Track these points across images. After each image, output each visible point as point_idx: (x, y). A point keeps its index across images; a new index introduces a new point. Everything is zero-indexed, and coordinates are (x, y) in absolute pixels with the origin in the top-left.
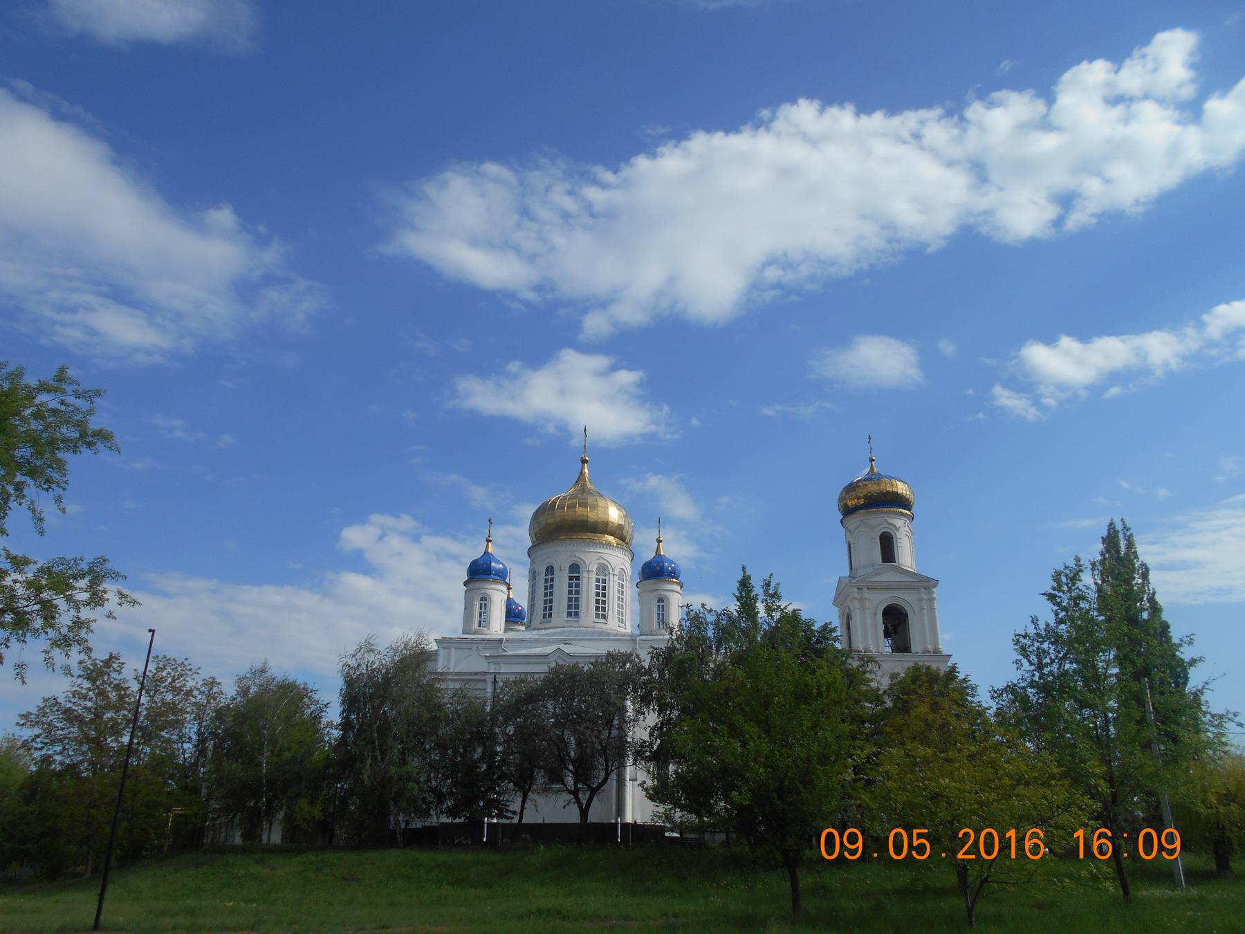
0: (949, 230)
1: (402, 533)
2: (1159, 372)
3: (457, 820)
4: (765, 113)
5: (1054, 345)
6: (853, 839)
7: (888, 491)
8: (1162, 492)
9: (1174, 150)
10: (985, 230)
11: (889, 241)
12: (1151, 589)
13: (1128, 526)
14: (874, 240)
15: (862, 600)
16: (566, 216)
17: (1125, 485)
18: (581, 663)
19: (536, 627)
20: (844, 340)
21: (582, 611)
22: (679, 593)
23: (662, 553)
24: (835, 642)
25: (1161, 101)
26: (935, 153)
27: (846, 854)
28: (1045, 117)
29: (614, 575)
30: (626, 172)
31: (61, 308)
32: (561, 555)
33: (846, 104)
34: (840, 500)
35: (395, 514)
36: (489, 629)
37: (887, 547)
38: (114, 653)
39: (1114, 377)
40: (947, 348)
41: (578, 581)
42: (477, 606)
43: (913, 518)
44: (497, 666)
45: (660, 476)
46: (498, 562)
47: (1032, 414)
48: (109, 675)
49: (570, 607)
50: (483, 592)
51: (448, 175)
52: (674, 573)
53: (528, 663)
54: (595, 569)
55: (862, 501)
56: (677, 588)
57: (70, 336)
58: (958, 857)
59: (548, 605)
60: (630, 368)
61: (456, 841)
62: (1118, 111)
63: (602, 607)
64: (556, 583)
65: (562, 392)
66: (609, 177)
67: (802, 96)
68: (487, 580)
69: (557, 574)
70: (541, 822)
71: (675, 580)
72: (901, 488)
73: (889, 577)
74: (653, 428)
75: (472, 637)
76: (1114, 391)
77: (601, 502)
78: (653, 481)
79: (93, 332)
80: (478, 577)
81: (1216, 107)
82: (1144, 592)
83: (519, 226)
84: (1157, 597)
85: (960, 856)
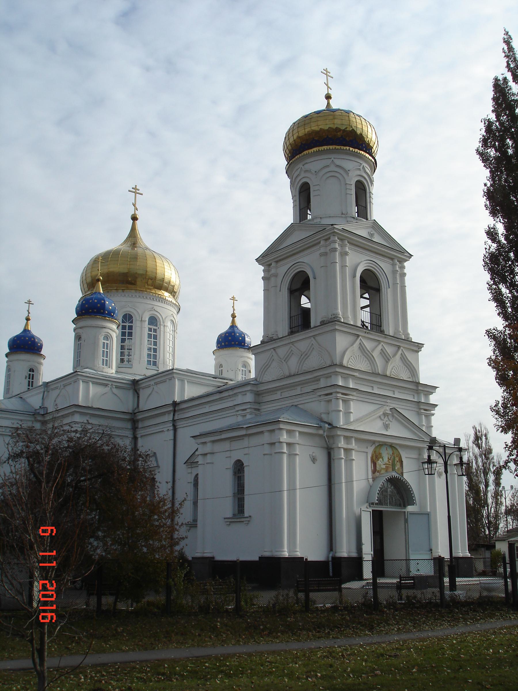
63: (125, 349)
69: (136, 325)
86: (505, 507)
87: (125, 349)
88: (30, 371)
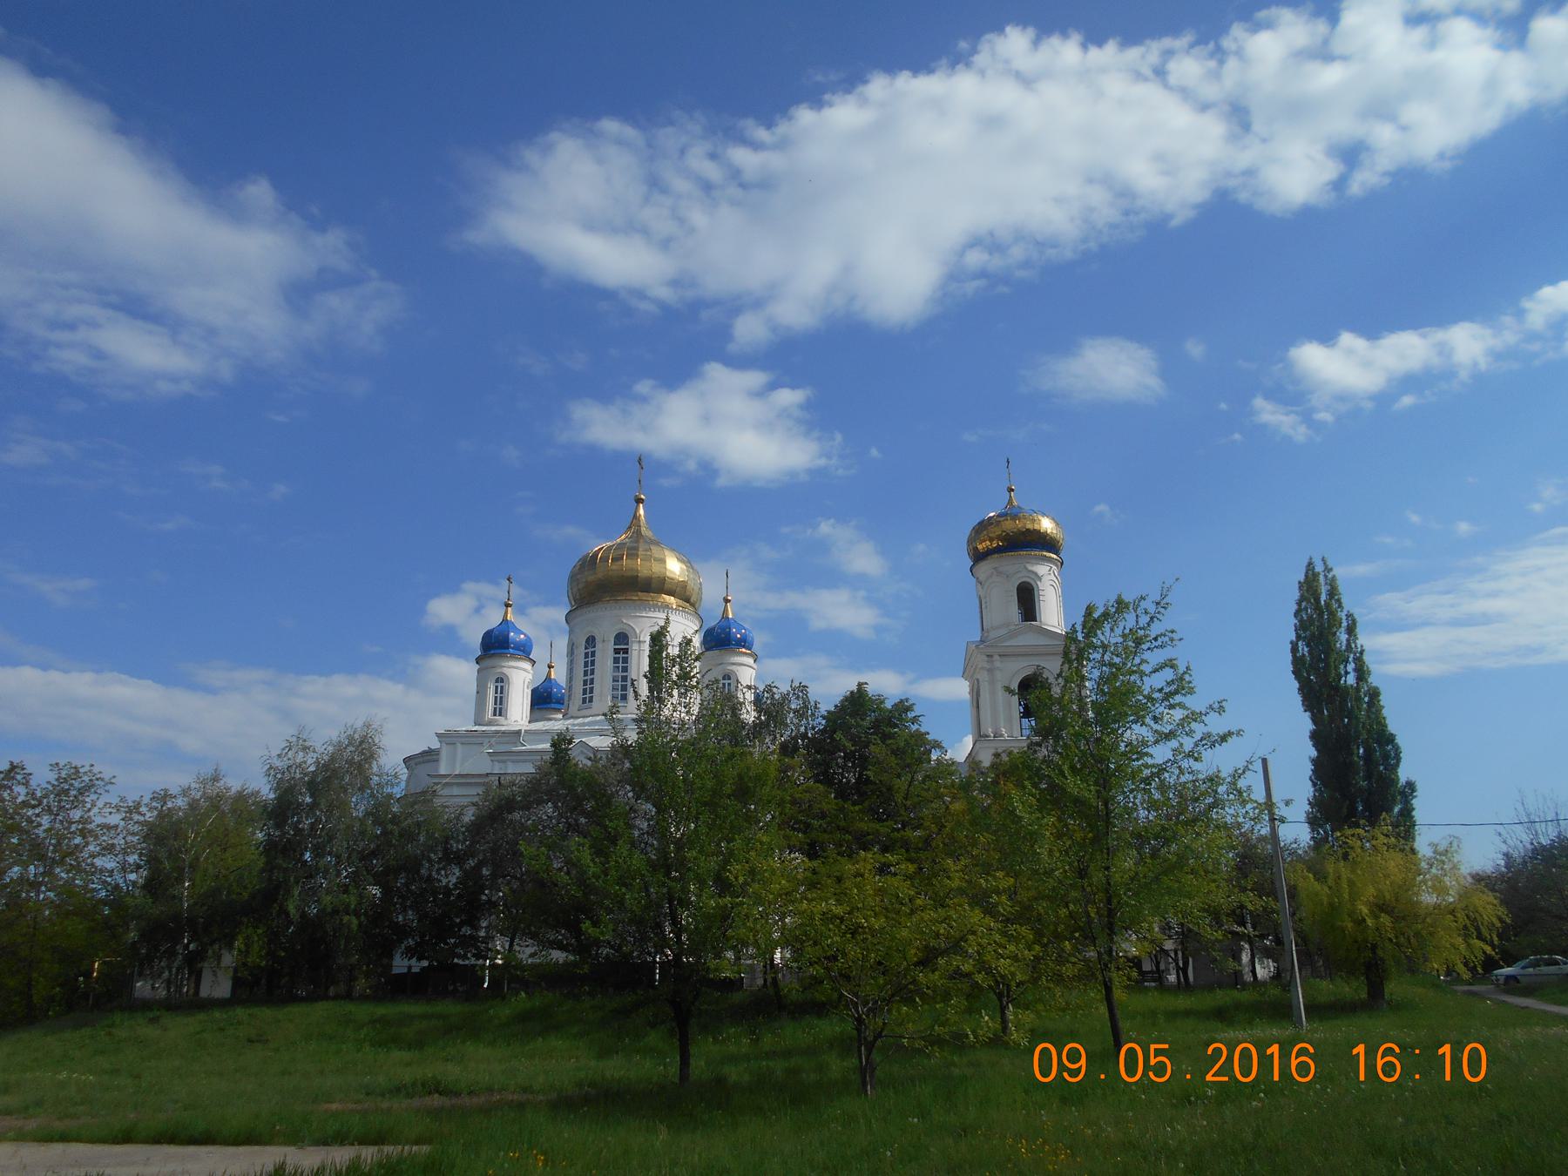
2: (1464, 375)
4: (963, 45)
6: (1074, 1056)
7: (1027, 529)
8: (1464, 527)
9: (1492, 84)
10: (1243, 197)
11: (1127, 213)
12: (1359, 646)
13: (1330, 567)
14: (1106, 211)
15: (990, 671)
16: (707, 187)
17: (1415, 519)
19: (574, 715)
20: (1066, 345)
23: (730, 616)
24: (913, 724)
25: (1479, 17)
26: (1184, 93)
27: (1065, 1074)
28: (1326, 41)
29: (673, 646)
30: (782, 128)
31: (55, 324)
32: (605, 621)
36: (506, 719)
38: (16, 761)
39: (1410, 382)
40: (1195, 349)
43: (1062, 564)
44: (502, 765)
45: (832, 521)
48: (11, 790)
50: (499, 671)
51: (554, 136)
56: (750, 661)
57: (70, 359)
58: (1207, 1079)
62: (1420, 33)
65: (707, 419)
66: (762, 134)
68: (503, 656)
69: (599, 646)
71: (744, 650)
73: (1028, 640)
74: (822, 462)
75: (484, 728)
76: (1407, 400)
78: (825, 528)
79: (99, 355)
80: (492, 652)
83: (647, 200)
84: (1365, 658)
85: (1209, 1078)
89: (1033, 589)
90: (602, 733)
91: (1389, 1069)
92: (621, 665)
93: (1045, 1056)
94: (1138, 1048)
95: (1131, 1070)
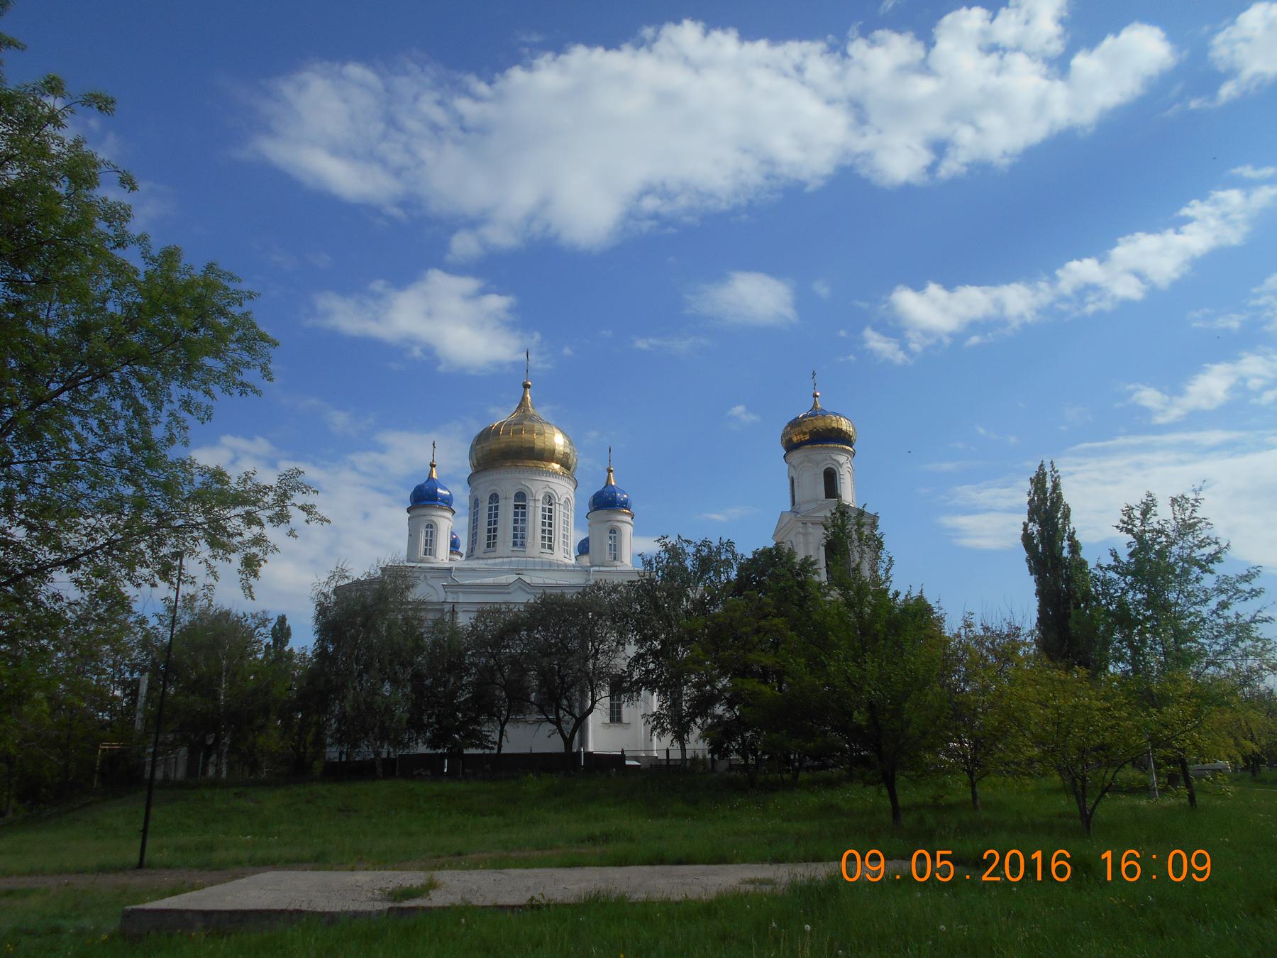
0: (827, 169)
1: (257, 457)
2: (1016, 324)
3: (440, 751)
4: (648, 32)
5: (922, 292)
6: (1201, 860)
8: (1013, 440)
9: (1041, 105)
10: (864, 172)
14: (754, 176)
15: (806, 535)
16: (435, 128)
17: (982, 431)
18: (570, 593)
20: (719, 275)
21: (529, 541)
22: (629, 524)
23: (613, 483)
26: (816, 89)
27: (1194, 875)
29: (560, 504)
30: (501, 84)
32: (506, 482)
33: (621, 46)
34: (784, 435)
35: (250, 437)
36: (435, 557)
37: (831, 481)
39: (975, 326)
40: (822, 289)
41: (524, 510)
42: (421, 534)
44: (455, 596)
46: (445, 489)
47: (900, 357)
49: (515, 536)
51: (306, 76)
52: (626, 504)
53: (478, 593)
54: (541, 498)
55: (807, 437)
56: (629, 519)
58: (983, 879)
59: (492, 534)
60: (500, 293)
61: (415, 773)
62: (993, 59)
63: (517, 538)
64: (500, 511)
66: (482, 88)
67: (687, 17)
68: (433, 507)
69: (501, 503)
70: (529, 752)
71: (627, 511)
72: (845, 425)
75: (419, 565)
76: (975, 340)
77: (547, 430)
81: (1083, 63)
82: (1065, 531)
83: (385, 137)
84: (1077, 537)
85: (985, 878)
86: (205, 563)
87: (517, 538)
88: (610, 532)
89: (836, 474)
90: (517, 572)
91: (1131, 871)
92: (520, 518)
93: (1178, 860)
94: (927, 854)
95: (1178, 872)
